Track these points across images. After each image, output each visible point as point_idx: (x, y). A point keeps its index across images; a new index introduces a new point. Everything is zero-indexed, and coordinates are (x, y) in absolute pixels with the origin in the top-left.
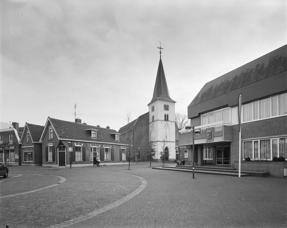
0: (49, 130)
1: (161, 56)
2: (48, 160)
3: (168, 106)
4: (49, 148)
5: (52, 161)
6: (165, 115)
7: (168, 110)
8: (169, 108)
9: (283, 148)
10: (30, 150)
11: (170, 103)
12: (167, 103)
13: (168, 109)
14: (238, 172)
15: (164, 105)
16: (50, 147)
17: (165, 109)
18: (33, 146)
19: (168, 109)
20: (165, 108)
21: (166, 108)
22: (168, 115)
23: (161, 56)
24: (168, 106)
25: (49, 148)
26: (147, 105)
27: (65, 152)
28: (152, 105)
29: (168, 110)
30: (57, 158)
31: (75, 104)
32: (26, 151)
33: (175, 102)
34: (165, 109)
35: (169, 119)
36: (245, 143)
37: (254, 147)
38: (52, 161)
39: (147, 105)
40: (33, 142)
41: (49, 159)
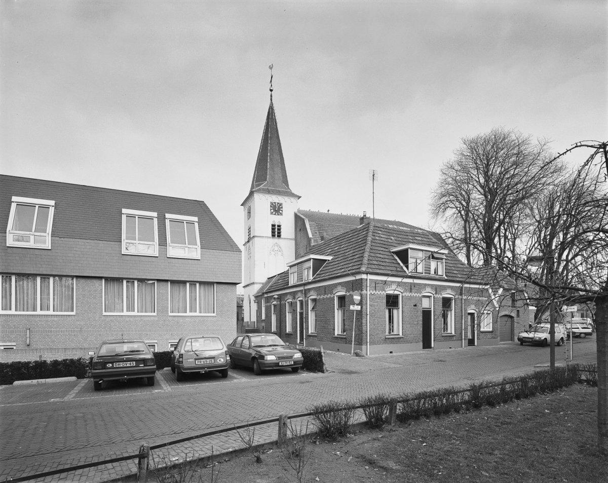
1: (271, 96)
3: (281, 204)
6: (273, 225)
7: (281, 214)
8: (282, 211)
9: (129, 304)
11: (286, 198)
12: (276, 199)
13: (281, 212)
14: (142, 312)
15: (271, 203)
17: (274, 213)
19: (281, 212)
20: (272, 211)
21: (275, 210)
22: (279, 226)
23: (271, 96)
24: (281, 204)
29: (281, 214)
32: (130, 308)
33: (299, 197)
34: (274, 213)
35: (282, 234)
37: (11, 285)
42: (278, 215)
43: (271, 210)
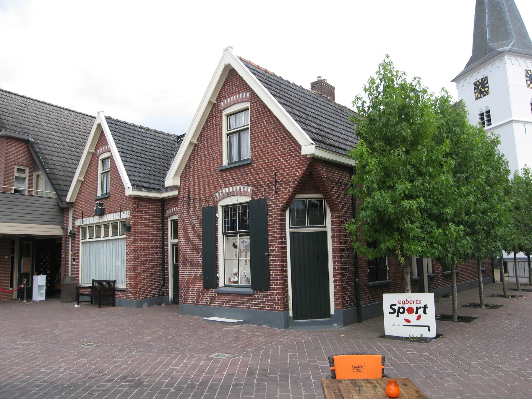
0: (100, 163)
2: (217, 278)
4: (220, 214)
5: (250, 291)
10: (95, 235)
16: (229, 210)
18: (126, 215)
19: (480, 82)
25: (220, 214)
26: (453, 81)
27: (325, 233)
28: (478, 76)
30: (284, 270)
31: (403, 326)
36: (233, 118)
38: (250, 291)
39: (453, 81)
40: (129, 191)
41: (220, 275)
43: (527, 81)
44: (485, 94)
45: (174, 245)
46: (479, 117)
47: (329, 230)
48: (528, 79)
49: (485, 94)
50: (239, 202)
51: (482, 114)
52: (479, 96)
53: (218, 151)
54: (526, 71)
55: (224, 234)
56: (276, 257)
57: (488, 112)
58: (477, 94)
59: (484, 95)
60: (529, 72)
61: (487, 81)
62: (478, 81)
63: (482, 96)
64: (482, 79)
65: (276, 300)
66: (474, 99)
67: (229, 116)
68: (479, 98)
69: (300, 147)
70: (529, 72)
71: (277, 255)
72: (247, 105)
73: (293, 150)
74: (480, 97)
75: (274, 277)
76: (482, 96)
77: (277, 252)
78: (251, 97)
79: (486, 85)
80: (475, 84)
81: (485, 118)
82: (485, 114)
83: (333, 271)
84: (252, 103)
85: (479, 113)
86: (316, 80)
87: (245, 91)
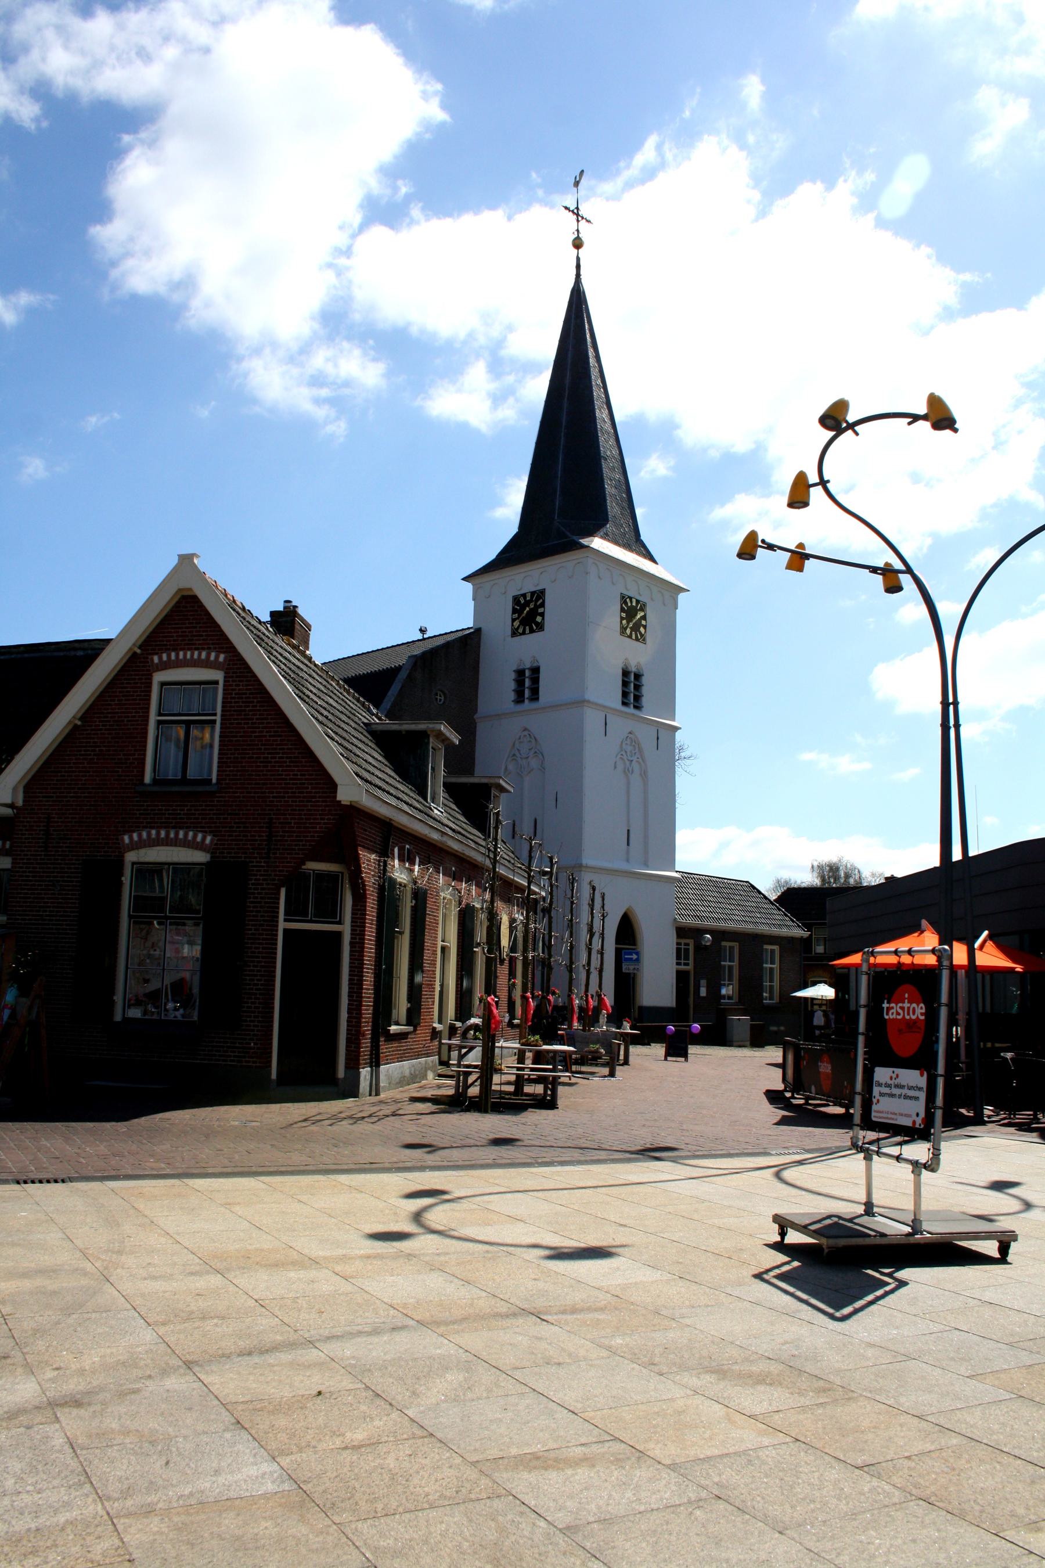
6: (625, 673)
13: (642, 630)
22: (638, 676)
26: (465, 579)
27: (339, 935)
39: (465, 579)
42: (637, 639)
43: (622, 619)
44: (535, 627)
45: (774, 964)
46: (513, 676)
47: (282, 925)
48: (624, 615)
49: (535, 627)
50: (175, 859)
51: (520, 673)
52: (521, 630)
53: (135, 750)
54: (623, 597)
55: (130, 917)
56: (258, 971)
57: (536, 671)
58: (517, 624)
59: (532, 631)
60: (628, 600)
61: (544, 602)
62: (524, 595)
63: (527, 631)
64: (533, 593)
65: (251, 1048)
66: (509, 633)
67: (163, 684)
68: (521, 634)
69: (333, 786)
70: (628, 600)
71: (262, 967)
72: (218, 675)
73: (312, 784)
74: (524, 633)
75: (250, 1007)
76: (527, 631)
77: (261, 962)
78: (229, 665)
79: (541, 610)
80: (516, 600)
81: (527, 683)
82: (527, 673)
83: (347, 1002)
84: (229, 677)
85: (515, 668)
86: (280, 608)
87: (215, 648)
